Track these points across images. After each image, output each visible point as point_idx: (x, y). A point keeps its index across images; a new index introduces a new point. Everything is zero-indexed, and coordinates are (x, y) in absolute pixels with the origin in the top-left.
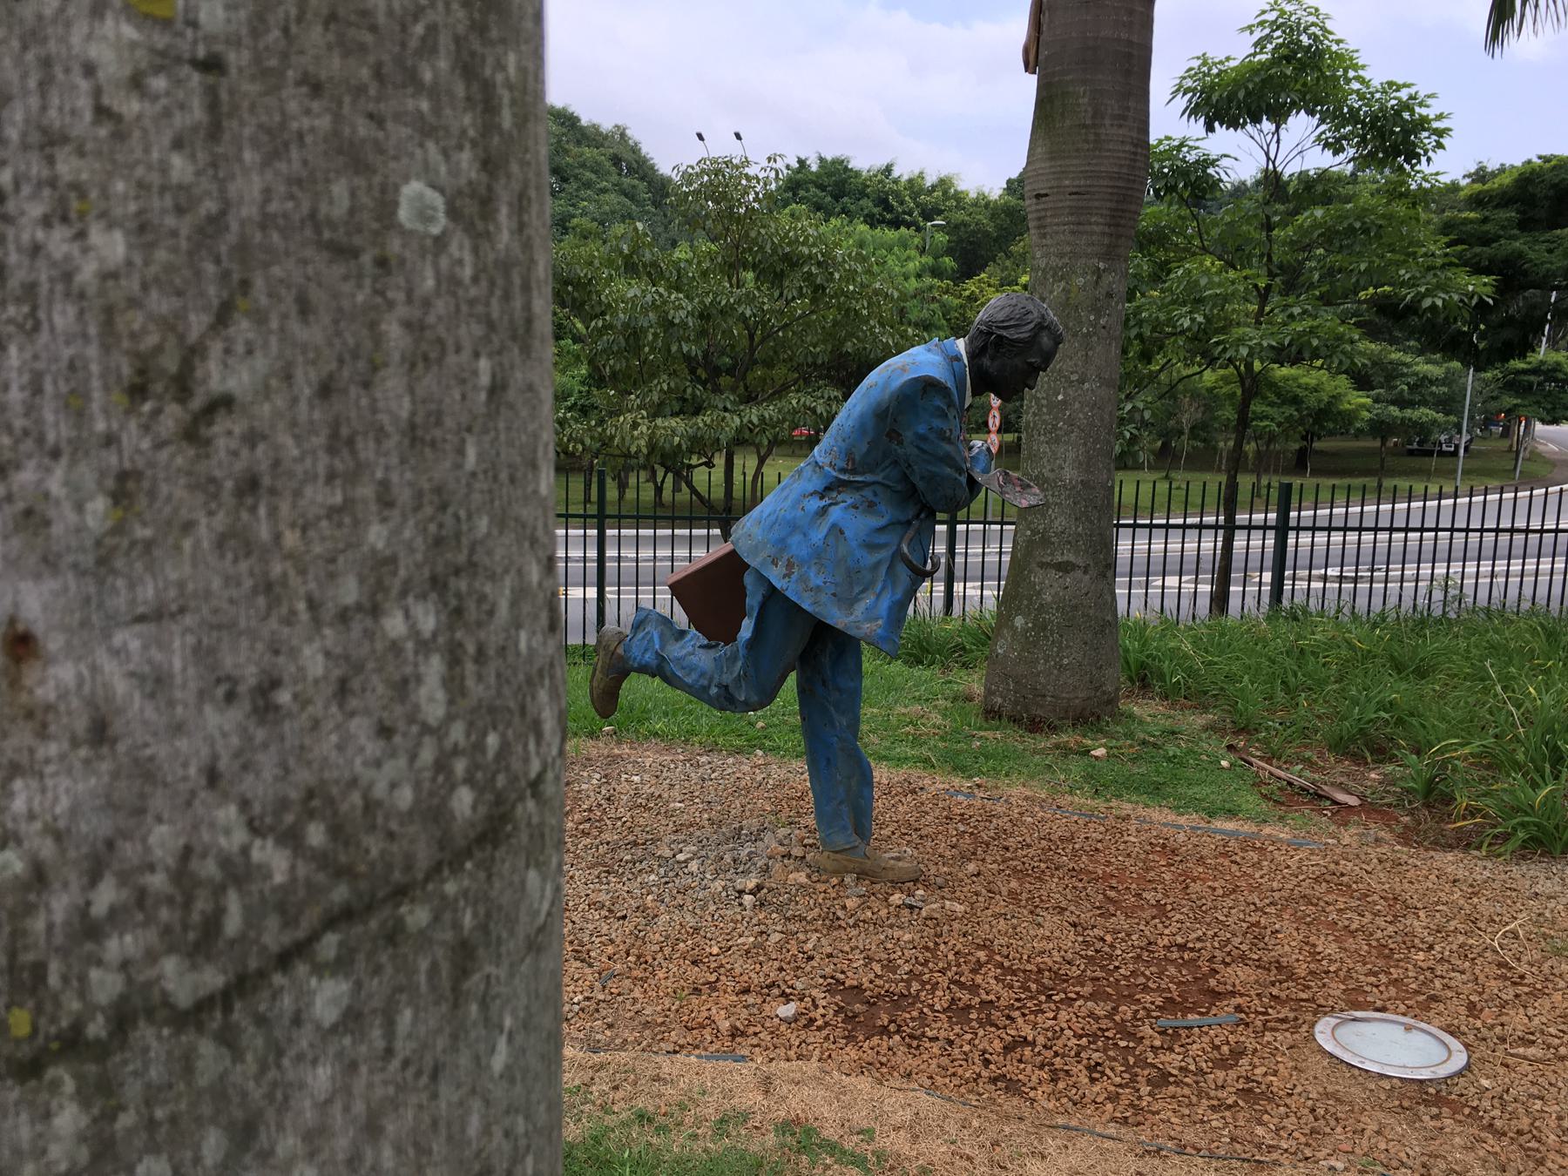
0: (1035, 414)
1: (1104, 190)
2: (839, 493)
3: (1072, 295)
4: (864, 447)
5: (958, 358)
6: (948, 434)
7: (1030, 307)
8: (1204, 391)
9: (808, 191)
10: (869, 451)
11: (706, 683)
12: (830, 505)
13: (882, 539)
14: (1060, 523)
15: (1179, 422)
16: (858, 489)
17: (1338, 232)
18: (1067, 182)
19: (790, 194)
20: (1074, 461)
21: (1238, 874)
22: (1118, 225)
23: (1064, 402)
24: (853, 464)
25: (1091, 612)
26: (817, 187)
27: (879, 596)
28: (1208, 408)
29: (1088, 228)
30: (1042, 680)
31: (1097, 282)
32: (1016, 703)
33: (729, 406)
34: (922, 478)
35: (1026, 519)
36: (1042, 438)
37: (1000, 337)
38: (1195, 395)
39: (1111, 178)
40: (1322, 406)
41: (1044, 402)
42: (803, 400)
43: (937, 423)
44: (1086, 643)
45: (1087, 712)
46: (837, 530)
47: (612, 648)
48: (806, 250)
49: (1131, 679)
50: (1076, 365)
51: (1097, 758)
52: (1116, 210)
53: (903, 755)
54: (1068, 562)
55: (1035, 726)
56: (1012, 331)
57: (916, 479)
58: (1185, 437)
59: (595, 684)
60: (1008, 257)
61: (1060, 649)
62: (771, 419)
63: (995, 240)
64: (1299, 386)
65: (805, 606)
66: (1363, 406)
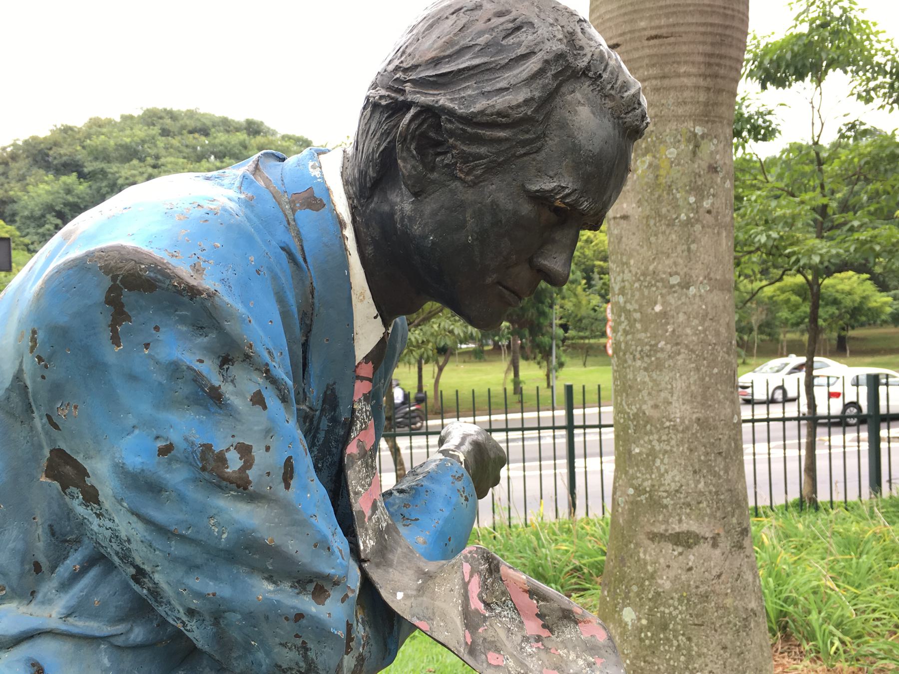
0: (626, 333)
1: (693, 29)
6: (234, 462)
8: (766, 299)
14: (673, 478)
15: (749, 323)
17: (882, 158)
18: (643, 24)
20: (685, 393)
22: (716, 76)
23: (664, 314)
25: (729, 602)
28: (769, 311)
29: (675, 82)
31: (694, 153)
35: (626, 473)
37: (429, 112)
38: (760, 303)
39: (702, 13)
40: (856, 305)
41: (637, 316)
44: (724, 648)
50: (675, 264)
52: (711, 55)
53: (686, 253)
54: (689, 534)
56: (469, 89)
57: (176, 616)
58: (755, 333)
61: (690, 658)
62: (417, 342)
64: (837, 291)
66: (885, 303)
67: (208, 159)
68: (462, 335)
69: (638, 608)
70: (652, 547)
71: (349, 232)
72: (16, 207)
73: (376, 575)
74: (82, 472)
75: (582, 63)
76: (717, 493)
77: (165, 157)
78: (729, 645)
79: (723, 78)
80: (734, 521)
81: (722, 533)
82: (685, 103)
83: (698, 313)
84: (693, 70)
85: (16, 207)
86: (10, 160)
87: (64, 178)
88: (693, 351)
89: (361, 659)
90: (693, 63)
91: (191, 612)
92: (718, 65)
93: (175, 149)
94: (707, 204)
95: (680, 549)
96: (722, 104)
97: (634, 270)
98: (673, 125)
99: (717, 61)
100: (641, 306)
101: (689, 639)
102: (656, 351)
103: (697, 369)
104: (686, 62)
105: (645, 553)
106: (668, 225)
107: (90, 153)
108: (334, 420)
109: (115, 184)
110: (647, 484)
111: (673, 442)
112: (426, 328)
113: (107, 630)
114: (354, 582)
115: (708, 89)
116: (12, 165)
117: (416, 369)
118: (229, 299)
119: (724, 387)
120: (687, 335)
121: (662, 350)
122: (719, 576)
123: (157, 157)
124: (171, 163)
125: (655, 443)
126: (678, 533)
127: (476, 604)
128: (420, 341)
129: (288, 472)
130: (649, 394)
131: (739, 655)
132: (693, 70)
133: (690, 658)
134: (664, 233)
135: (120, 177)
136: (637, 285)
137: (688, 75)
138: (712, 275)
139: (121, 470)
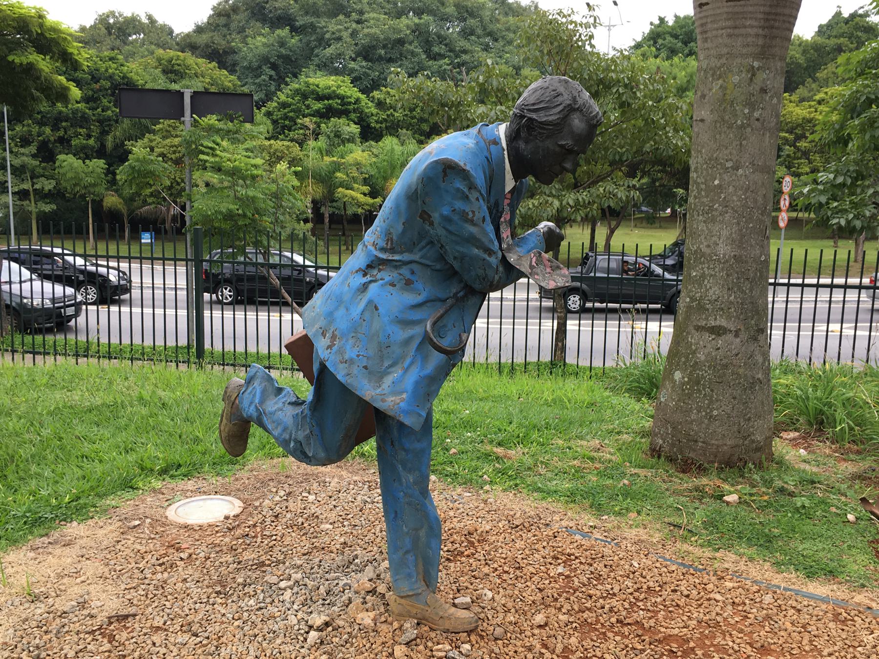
0: (695, 197)
2: (380, 270)
3: (728, 92)
4: (400, 228)
5: (496, 142)
6: (471, 214)
7: (561, 89)
9: (664, 39)
10: (404, 232)
11: (287, 437)
12: (371, 282)
13: (416, 315)
16: (396, 267)
19: (652, 42)
20: (728, 238)
21: (807, 648)
22: (772, 27)
23: (720, 186)
24: (392, 244)
25: (741, 371)
26: (672, 36)
27: (406, 370)
30: (695, 428)
31: (751, 79)
32: (673, 445)
33: (554, 192)
34: (455, 258)
36: (701, 218)
37: (531, 119)
41: (703, 186)
42: (608, 187)
43: (459, 205)
44: (734, 398)
45: (735, 458)
46: (372, 306)
47: (233, 398)
48: (614, 75)
49: (810, 424)
50: (731, 154)
51: (728, 503)
52: (769, 14)
54: (720, 327)
55: (686, 467)
56: (542, 114)
57: (450, 260)
59: (222, 428)
60: (814, 81)
61: (711, 402)
63: (806, 69)
65: (339, 377)
67: (407, 15)
68: (624, 198)
69: (683, 371)
70: (696, 334)
71: (506, 152)
72: (237, 57)
73: (506, 254)
74: (430, 216)
75: (577, 106)
76: (742, 304)
77: (369, 13)
78: (738, 397)
79: (777, 28)
80: (753, 322)
81: (742, 329)
82: (748, 46)
83: (742, 187)
84: (755, 23)
85: (237, 57)
86: (232, 13)
87: (279, 32)
88: (736, 212)
89: (500, 278)
90: (756, 19)
91: (455, 258)
92: (775, 20)
93: (377, 5)
94: (756, 114)
95: (713, 337)
96: (775, 46)
97: (704, 156)
98: (739, 60)
99: (773, 17)
100: (706, 180)
101: (712, 391)
102: (712, 210)
103: (738, 224)
104: (751, 18)
105: (692, 338)
106: (728, 128)
107: (302, 7)
108: (497, 211)
109: (322, 38)
110: (698, 295)
111: (717, 270)
112: (593, 190)
113: (430, 264)
114: (500, 254)
115: (765, 36)
116: (234, 17)
117: (589, 231)
118: (473, 172)
119: (756, 237)
120: (733, 201)
121: (716, 209)
122: (737, 355)
123: (361, 13)
124: (373, 19)
125: (705, 269)
126: (713, 327)
127: (534, 263)
128: (587, 202)
129: (484, 220)
130: (705, 238)
131: (744, 403)
132: (755, 23)
133: (711, 402)
134: (725, 132)
135: (328, 31)
136: (705, 166)
137: (752, 27)
138: (755, 162)
139: (442, 216)
